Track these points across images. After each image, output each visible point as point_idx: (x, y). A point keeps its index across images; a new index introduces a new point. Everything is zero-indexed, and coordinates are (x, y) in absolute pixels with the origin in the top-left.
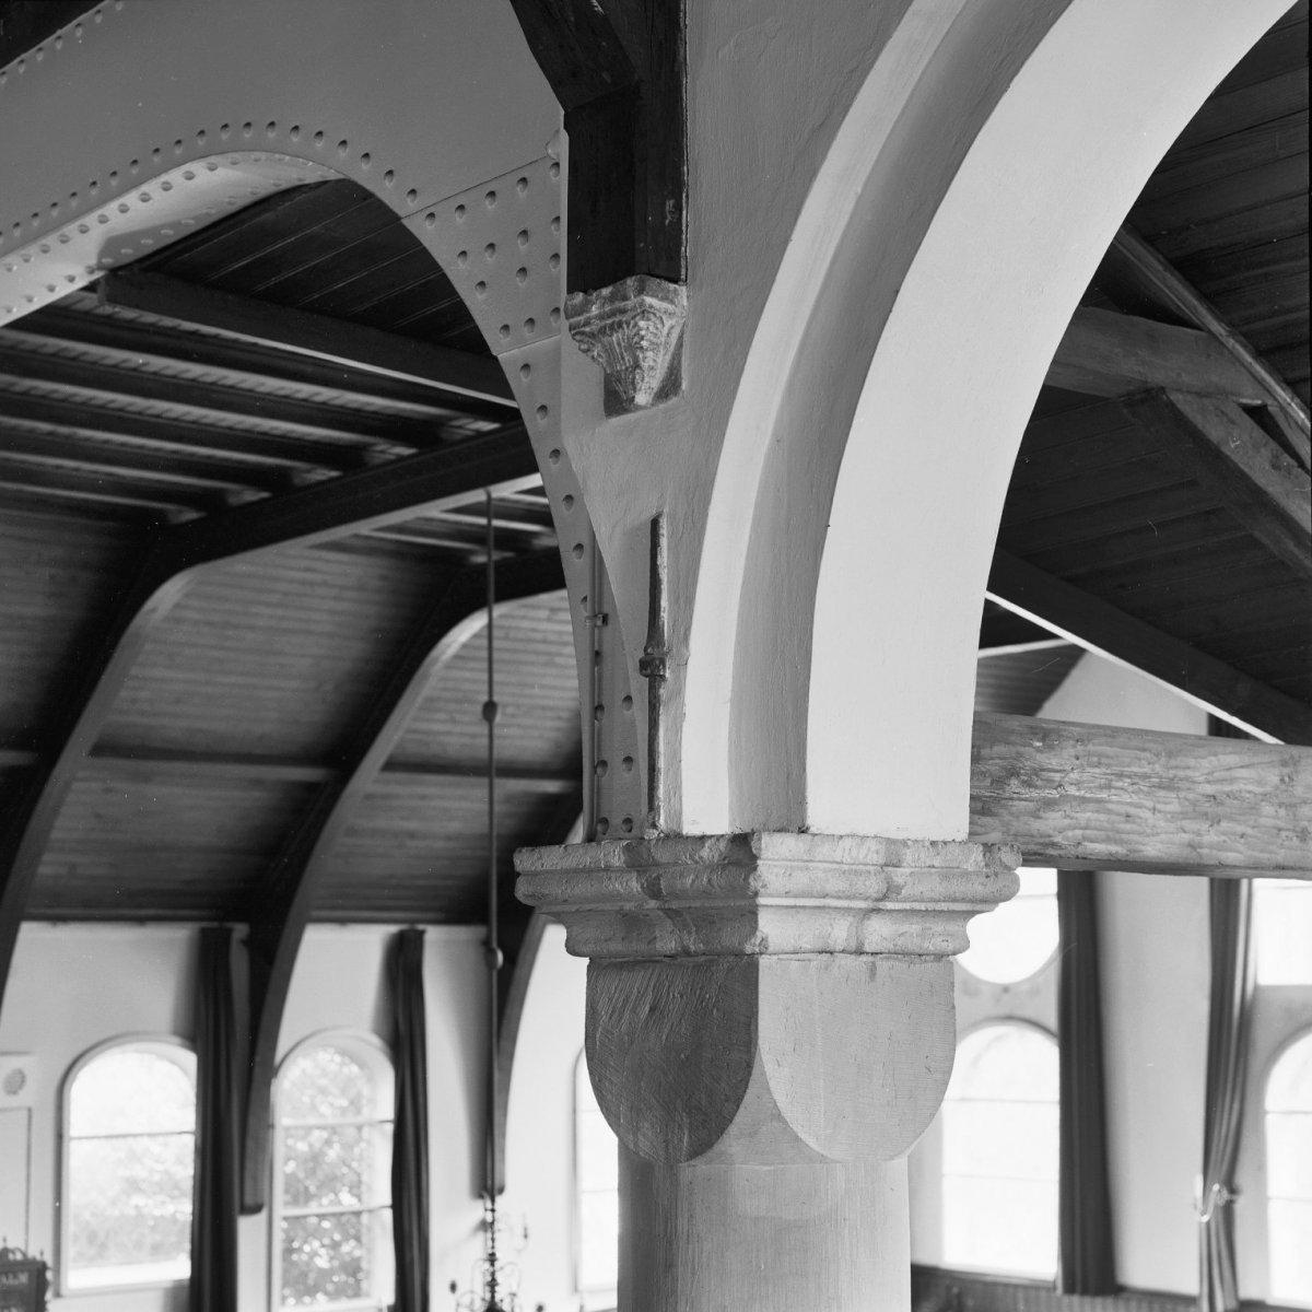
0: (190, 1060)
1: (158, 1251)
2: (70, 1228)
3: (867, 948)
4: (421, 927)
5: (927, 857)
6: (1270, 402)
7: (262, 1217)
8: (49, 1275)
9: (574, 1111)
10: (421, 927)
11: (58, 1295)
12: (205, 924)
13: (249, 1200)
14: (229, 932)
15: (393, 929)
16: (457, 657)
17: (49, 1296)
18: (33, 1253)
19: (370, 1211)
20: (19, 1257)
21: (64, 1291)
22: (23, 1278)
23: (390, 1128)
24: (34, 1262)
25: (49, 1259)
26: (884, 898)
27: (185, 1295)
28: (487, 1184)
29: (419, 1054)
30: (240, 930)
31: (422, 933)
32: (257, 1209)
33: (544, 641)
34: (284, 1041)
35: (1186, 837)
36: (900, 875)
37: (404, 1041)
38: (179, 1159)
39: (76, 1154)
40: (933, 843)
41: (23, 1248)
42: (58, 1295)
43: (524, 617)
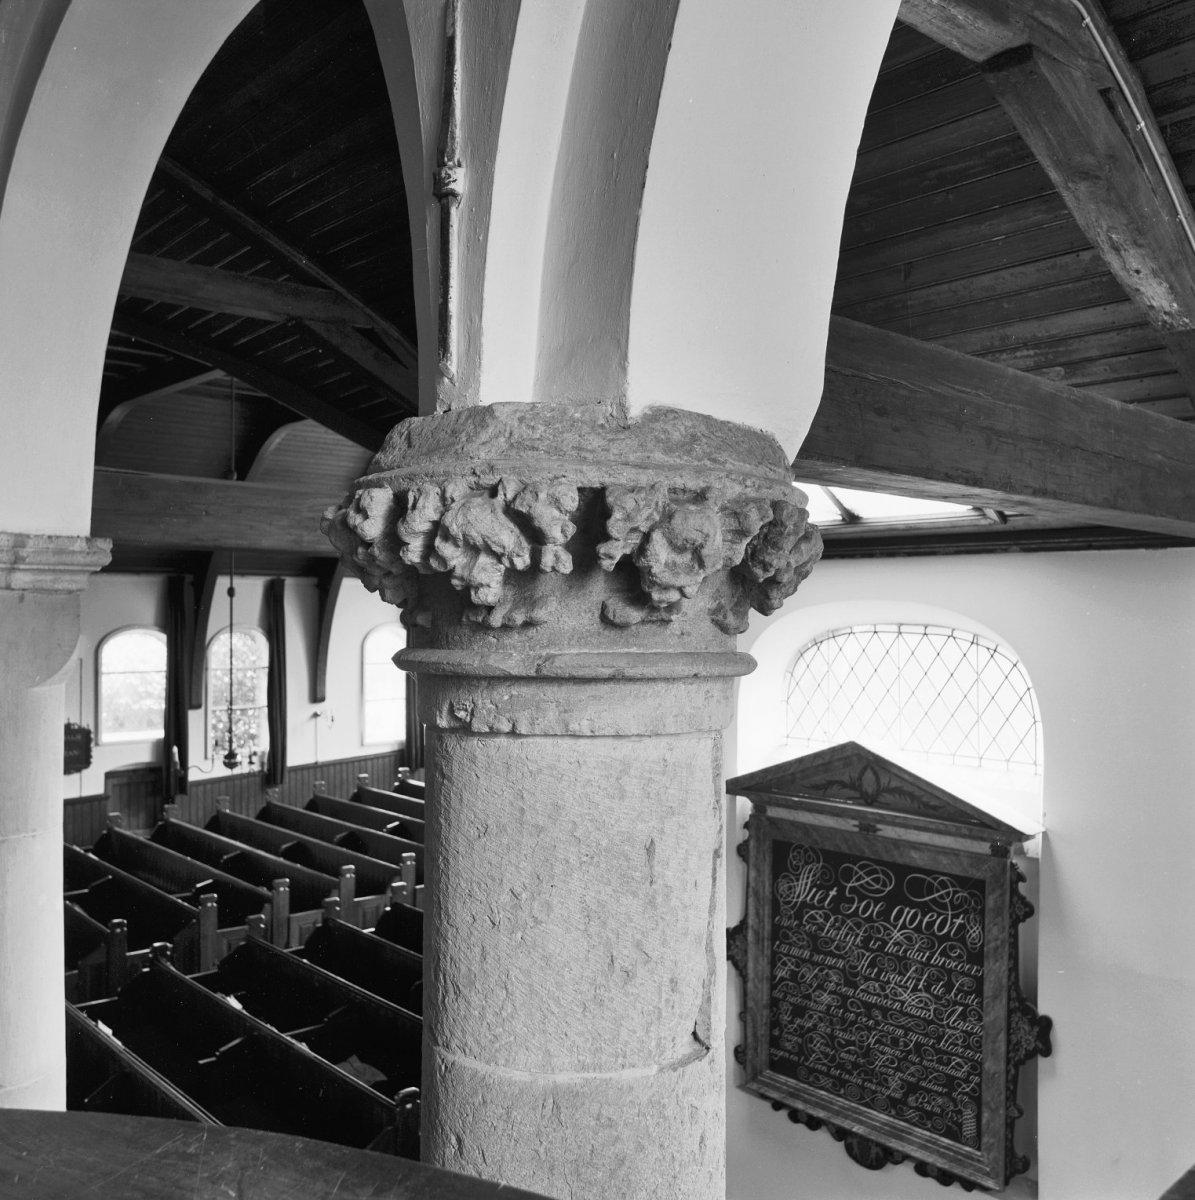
0: (164, 637)
1: (151, 724)
2: (104, 715)
3: (13, 586)
4: (283, 578)
5: (42, 544)
6: (376, 326)
7: (201, 711)
8: (92, 736)
9: (362, 663)
10: (283, 578)
11: (97, 744)
12: (269, 578)
13: (194, 702)
14: (184, 578)
15: (269, 578)
16: (276, 449)
17: (92, 745)
18: (84, 725)
19: (259, 708)
20: (76, 727)
21: (100, 743)
22: (79, 737)
23: (267, 670)
24: (84, 729)
25: (92, 728)
26: (15, 562)
27: (162, 745)
28: (316, 695)
29: (281, 639)
30: (189, 578)
31: (283, 581)
32: (198, 706)
33: (325, 443)
34: (210, 634)
35: (293, 537)
36: (23, 553)
37: (274, 630)
38: (159, 684)
39: (104, 680)
40: (50, 537)
41: (78, 723)
42: (97, 744)
43: (313, 431)
